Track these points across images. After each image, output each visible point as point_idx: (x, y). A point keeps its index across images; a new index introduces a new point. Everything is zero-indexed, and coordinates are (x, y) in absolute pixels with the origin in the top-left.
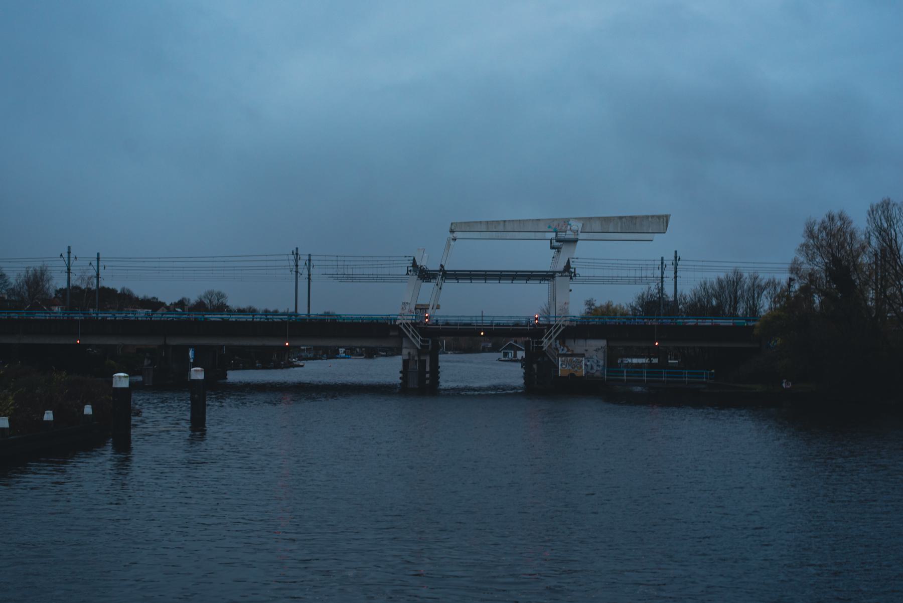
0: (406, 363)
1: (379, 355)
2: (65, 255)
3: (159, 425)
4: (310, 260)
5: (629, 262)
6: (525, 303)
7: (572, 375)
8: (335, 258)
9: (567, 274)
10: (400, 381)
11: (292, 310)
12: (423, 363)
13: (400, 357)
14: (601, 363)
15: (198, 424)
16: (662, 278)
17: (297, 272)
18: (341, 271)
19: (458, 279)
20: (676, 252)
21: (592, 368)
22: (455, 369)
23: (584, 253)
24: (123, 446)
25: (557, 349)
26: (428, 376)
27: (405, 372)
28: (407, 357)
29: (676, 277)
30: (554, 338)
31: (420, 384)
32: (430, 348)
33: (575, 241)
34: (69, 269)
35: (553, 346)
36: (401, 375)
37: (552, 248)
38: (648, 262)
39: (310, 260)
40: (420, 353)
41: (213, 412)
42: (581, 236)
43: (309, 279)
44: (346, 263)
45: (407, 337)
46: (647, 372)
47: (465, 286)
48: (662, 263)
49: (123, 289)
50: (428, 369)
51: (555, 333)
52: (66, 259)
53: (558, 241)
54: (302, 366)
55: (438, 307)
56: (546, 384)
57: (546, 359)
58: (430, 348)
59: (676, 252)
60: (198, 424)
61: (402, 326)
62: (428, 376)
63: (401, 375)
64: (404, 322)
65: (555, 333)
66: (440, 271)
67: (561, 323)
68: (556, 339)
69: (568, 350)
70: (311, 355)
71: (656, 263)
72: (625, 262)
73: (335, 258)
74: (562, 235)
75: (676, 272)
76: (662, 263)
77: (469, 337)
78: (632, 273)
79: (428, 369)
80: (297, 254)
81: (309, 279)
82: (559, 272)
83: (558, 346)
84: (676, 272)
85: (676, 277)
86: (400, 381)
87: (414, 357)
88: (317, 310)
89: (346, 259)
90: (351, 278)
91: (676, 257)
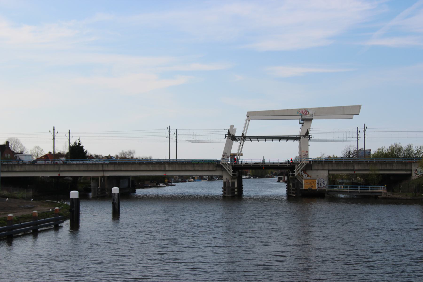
0: (225, 183)
1: (215, 180)
2: (52, 131)
3: (94, 216)
4: (176, 132)
5: (322, 130)
6: (287, 152)
7: (310, 189)
8: (189, 131)
9: (307, 137)
10: (222, 193)
11: (167, 158)
12: (233, 184)
13: (222, 181)
14: (326, 182)
15: (116, 214)
16: (358, 138)
17: (170, 138)
18: (192, 137)
19: (265, 140)
20: (364, 124)
21: (321, 185)
22: (251, 187)
23: (317, 126)
24: (75, 227)
25: (302, 175)
26: (236, 190)
27: (224, 188)
28: (225, 181)
29: (365, 138)
30: (300, 169)
31: (233, 195)
32: (237, 175)
33: (311, 120)
34: (54, 138)
35: (300, 174)
36: (223, 190)
37: (300, 123)
38: (349, 130)
39: (176, 132)
40: (232, 178)
41: (124, 208)
42: (314, 117)
43: (176, 141)
44: (195, 133)
45: (225, 170)
46: (350, 187)
47: (255, 143)
48: (358, 130)
49: (83, 147)
50: (236, 186)
51: (301, 167)
52: (53, 133)
53: (302, 120)
54: (175, 185)
55: (242, 155)
56: (299, 195)
57: (296, 181)
58: (237, 175)
59: (364, 124)
60: (116, 214)
61: (223, 165)
62: (236, 190)
63: (223, 190)
64: (224, 162)
65: (301, 167)
66: (242, 136)
67: (304, 162)
68: (302, 170)
69: (308, 176)
70: (410, 196)
71: (354, 130)
72: (320, 130)
73: (189, 131)
74: (304, 117)
75: (365, 135)
76: (358, 130)
77: (261, 170)
78: (342, 136)
79: (236, 186)
80: (170, 129)
81: (176, 141)
82: (303, 136)
83: (303, 174)
84: (365, 135)
85: (365, 138)
86: (222, 193)
87: (229, 180)
88: (57, 152)
89: (191, 131)
90: (197, 141)
91: (364, 127)
